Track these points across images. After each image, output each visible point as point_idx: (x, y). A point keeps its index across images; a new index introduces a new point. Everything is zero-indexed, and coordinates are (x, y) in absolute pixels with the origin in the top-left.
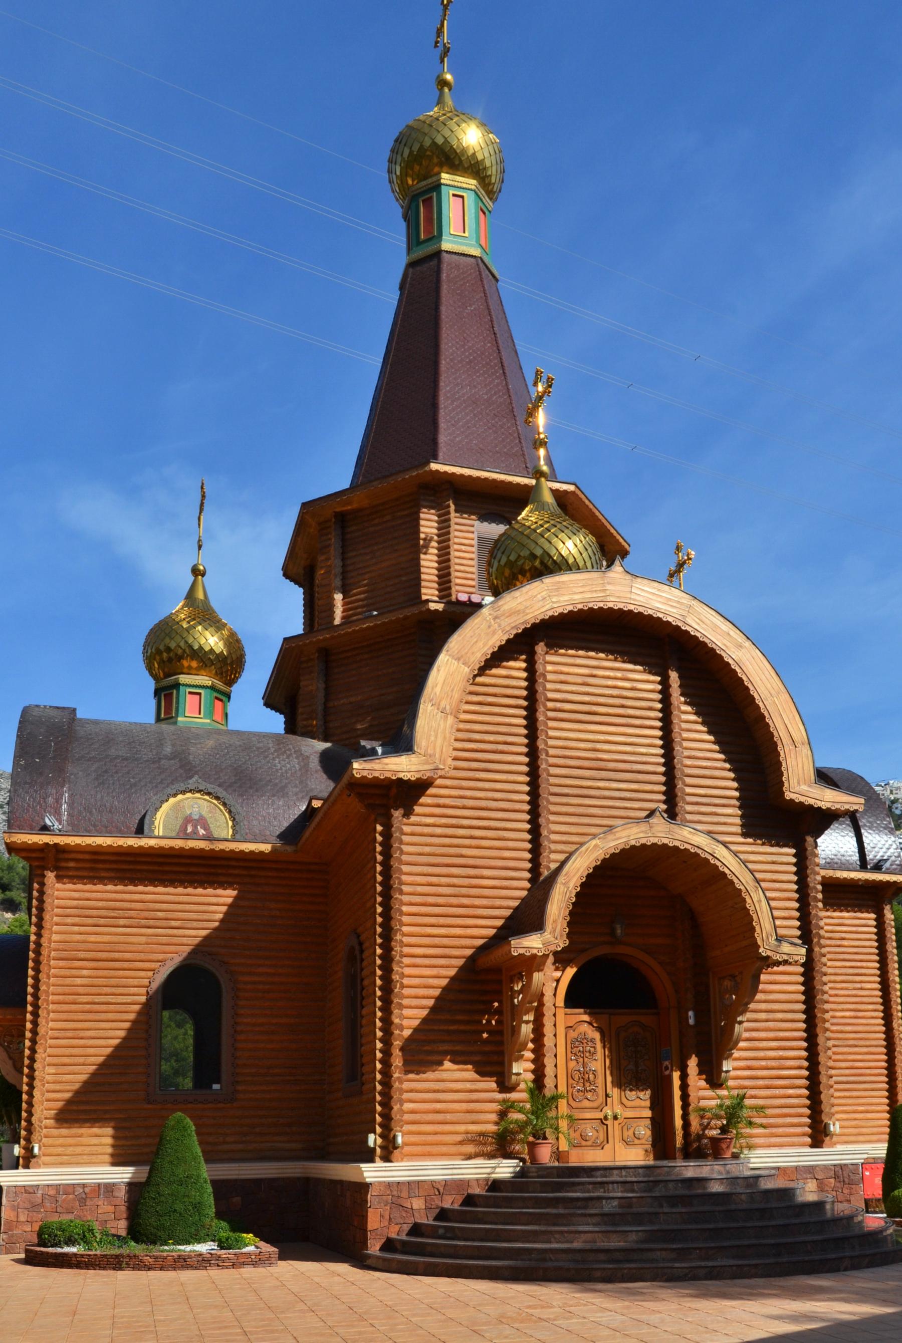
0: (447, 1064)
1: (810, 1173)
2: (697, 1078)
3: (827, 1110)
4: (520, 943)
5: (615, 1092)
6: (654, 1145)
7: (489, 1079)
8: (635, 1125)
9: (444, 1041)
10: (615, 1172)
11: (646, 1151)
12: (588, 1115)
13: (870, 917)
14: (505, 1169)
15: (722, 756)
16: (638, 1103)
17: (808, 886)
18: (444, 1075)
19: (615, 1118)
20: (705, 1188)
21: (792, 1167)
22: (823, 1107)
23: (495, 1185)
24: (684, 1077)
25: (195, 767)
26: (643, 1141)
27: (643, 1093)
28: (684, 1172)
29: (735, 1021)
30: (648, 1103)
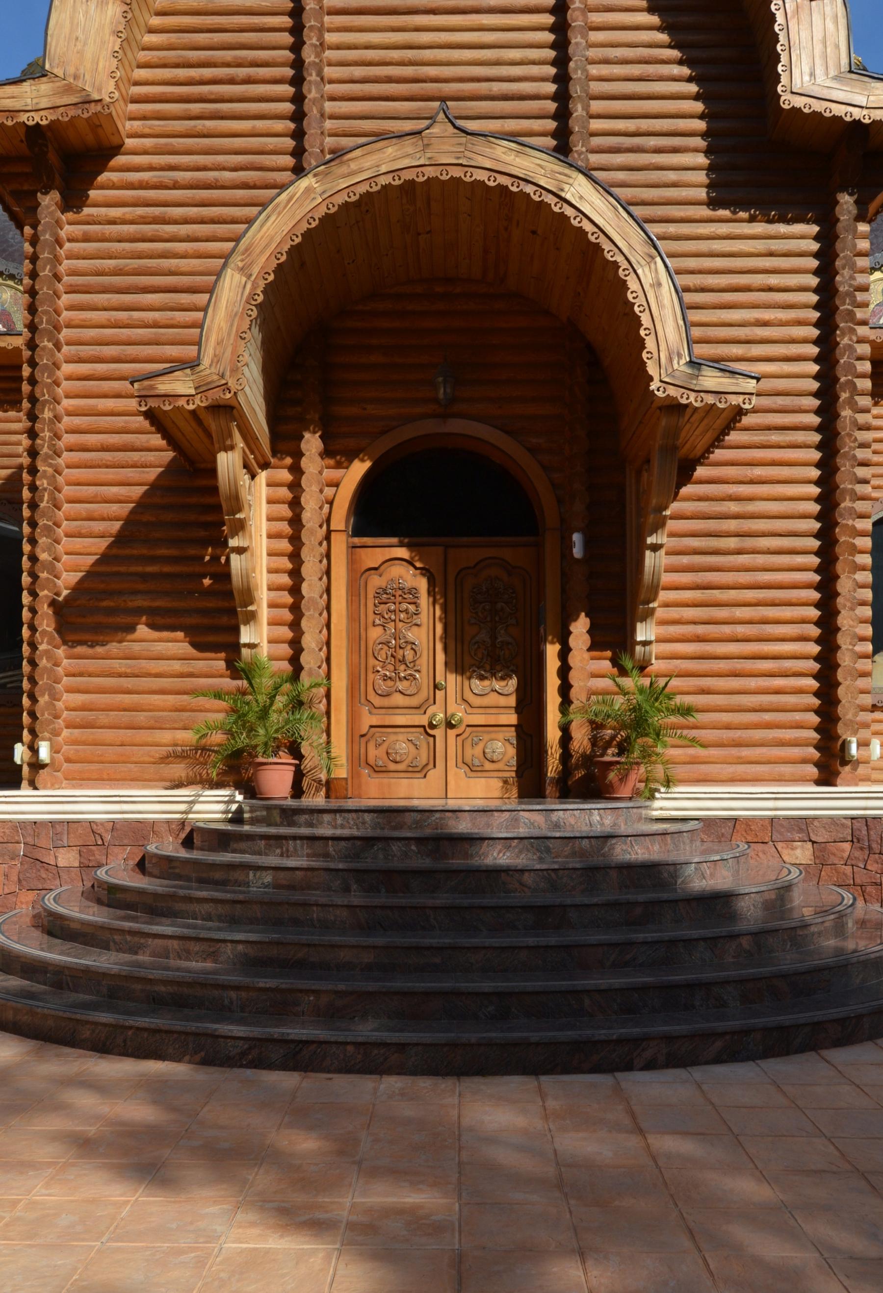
0: (142, 630)
1: (801, 830)
2: (587, 655)
3: (849, 716)
4: (152, 387)
5: (452, 681)
6: (520, 772)
7: (212, 655)
8: (486, 737)
9: (135, 592)
10: (327, 817)
11: (505, 782)
12: (400, 720)
13: (803, 235)
14: (212, 806)
15: (675, 54)
16: (493, 699)
17: (837, 291)
18: (136, 647)
19: (450, 725)
20: (467, 856)
21: (762, 819)
22: (840, 710)
23: (192, 836)
24: (564, 654)
25: (12, 246)
26: (500, 766)
27: (503, 683)
28: (451, 823)
29: (641, 548)
30: (512, 701)
